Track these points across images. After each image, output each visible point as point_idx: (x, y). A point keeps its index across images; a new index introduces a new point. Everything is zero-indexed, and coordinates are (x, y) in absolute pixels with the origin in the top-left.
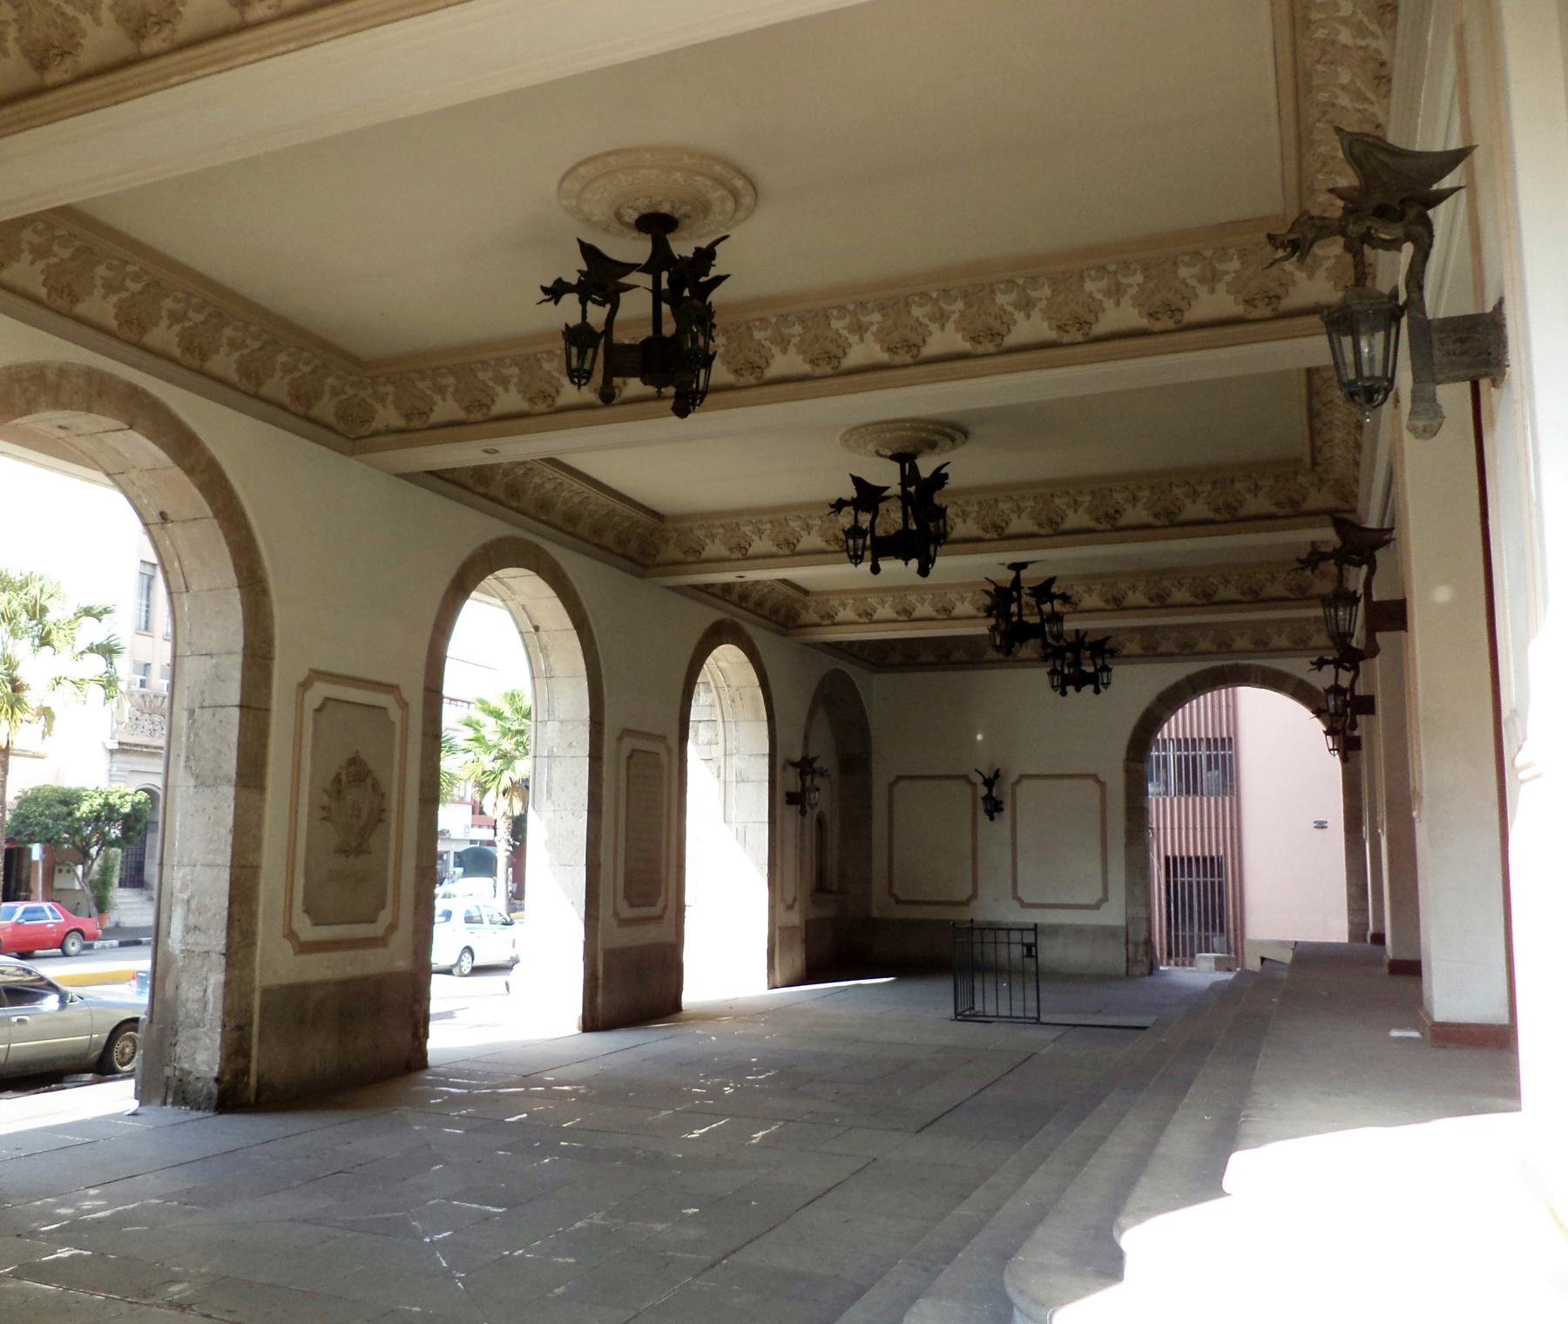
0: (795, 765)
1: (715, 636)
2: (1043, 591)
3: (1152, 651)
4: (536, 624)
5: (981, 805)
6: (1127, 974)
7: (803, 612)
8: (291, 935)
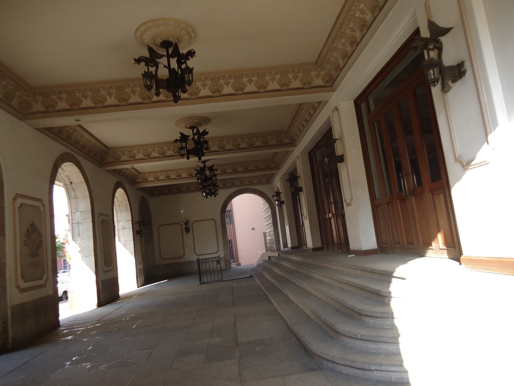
0: (138, 223)
1: (118, 185)
2: (211, 169)
3: (225, 187)
4: (71, 181)
5: (184, 230)
6: (226, 269)
7: (138, 179)
8: (18, 287)
